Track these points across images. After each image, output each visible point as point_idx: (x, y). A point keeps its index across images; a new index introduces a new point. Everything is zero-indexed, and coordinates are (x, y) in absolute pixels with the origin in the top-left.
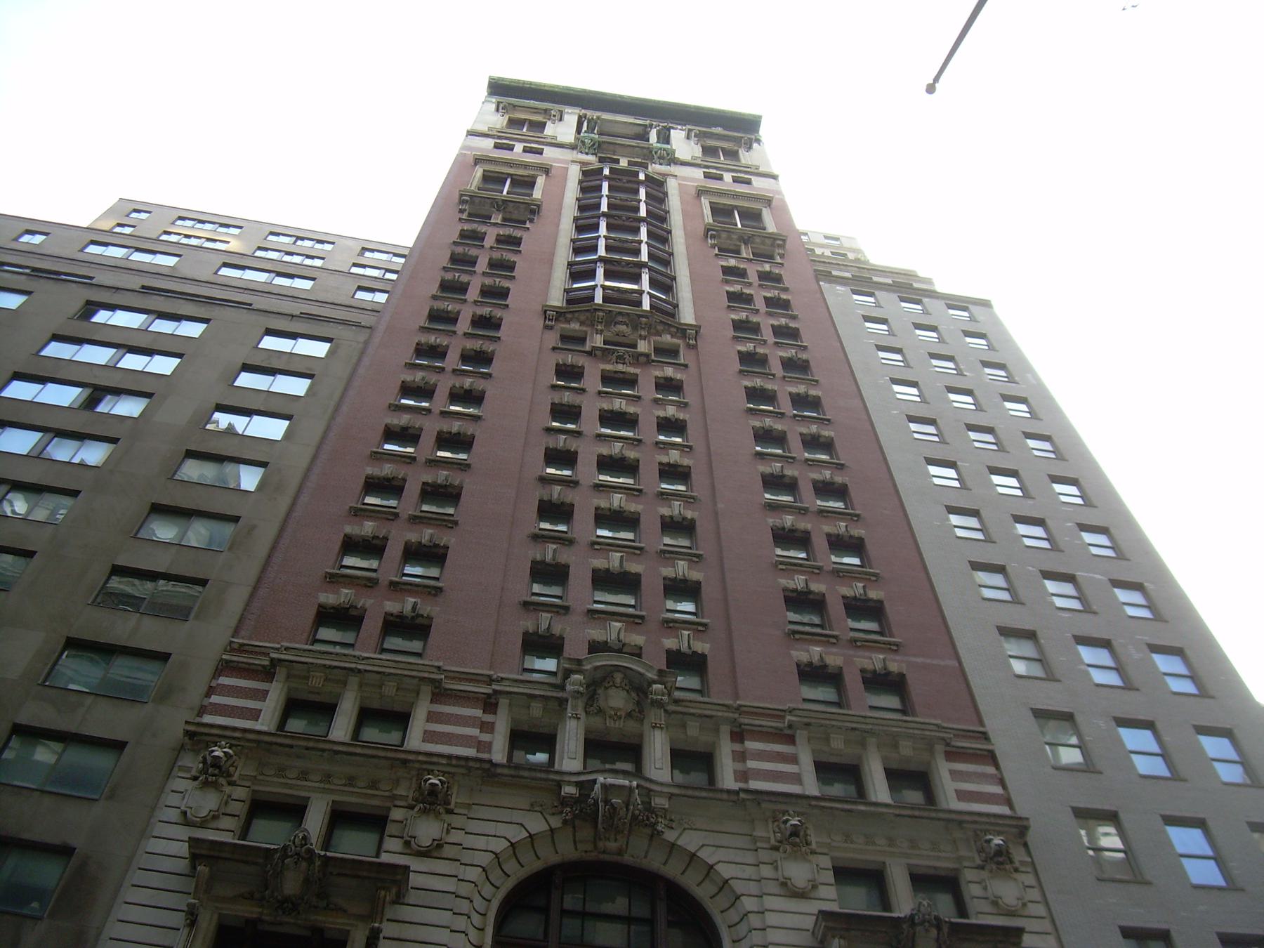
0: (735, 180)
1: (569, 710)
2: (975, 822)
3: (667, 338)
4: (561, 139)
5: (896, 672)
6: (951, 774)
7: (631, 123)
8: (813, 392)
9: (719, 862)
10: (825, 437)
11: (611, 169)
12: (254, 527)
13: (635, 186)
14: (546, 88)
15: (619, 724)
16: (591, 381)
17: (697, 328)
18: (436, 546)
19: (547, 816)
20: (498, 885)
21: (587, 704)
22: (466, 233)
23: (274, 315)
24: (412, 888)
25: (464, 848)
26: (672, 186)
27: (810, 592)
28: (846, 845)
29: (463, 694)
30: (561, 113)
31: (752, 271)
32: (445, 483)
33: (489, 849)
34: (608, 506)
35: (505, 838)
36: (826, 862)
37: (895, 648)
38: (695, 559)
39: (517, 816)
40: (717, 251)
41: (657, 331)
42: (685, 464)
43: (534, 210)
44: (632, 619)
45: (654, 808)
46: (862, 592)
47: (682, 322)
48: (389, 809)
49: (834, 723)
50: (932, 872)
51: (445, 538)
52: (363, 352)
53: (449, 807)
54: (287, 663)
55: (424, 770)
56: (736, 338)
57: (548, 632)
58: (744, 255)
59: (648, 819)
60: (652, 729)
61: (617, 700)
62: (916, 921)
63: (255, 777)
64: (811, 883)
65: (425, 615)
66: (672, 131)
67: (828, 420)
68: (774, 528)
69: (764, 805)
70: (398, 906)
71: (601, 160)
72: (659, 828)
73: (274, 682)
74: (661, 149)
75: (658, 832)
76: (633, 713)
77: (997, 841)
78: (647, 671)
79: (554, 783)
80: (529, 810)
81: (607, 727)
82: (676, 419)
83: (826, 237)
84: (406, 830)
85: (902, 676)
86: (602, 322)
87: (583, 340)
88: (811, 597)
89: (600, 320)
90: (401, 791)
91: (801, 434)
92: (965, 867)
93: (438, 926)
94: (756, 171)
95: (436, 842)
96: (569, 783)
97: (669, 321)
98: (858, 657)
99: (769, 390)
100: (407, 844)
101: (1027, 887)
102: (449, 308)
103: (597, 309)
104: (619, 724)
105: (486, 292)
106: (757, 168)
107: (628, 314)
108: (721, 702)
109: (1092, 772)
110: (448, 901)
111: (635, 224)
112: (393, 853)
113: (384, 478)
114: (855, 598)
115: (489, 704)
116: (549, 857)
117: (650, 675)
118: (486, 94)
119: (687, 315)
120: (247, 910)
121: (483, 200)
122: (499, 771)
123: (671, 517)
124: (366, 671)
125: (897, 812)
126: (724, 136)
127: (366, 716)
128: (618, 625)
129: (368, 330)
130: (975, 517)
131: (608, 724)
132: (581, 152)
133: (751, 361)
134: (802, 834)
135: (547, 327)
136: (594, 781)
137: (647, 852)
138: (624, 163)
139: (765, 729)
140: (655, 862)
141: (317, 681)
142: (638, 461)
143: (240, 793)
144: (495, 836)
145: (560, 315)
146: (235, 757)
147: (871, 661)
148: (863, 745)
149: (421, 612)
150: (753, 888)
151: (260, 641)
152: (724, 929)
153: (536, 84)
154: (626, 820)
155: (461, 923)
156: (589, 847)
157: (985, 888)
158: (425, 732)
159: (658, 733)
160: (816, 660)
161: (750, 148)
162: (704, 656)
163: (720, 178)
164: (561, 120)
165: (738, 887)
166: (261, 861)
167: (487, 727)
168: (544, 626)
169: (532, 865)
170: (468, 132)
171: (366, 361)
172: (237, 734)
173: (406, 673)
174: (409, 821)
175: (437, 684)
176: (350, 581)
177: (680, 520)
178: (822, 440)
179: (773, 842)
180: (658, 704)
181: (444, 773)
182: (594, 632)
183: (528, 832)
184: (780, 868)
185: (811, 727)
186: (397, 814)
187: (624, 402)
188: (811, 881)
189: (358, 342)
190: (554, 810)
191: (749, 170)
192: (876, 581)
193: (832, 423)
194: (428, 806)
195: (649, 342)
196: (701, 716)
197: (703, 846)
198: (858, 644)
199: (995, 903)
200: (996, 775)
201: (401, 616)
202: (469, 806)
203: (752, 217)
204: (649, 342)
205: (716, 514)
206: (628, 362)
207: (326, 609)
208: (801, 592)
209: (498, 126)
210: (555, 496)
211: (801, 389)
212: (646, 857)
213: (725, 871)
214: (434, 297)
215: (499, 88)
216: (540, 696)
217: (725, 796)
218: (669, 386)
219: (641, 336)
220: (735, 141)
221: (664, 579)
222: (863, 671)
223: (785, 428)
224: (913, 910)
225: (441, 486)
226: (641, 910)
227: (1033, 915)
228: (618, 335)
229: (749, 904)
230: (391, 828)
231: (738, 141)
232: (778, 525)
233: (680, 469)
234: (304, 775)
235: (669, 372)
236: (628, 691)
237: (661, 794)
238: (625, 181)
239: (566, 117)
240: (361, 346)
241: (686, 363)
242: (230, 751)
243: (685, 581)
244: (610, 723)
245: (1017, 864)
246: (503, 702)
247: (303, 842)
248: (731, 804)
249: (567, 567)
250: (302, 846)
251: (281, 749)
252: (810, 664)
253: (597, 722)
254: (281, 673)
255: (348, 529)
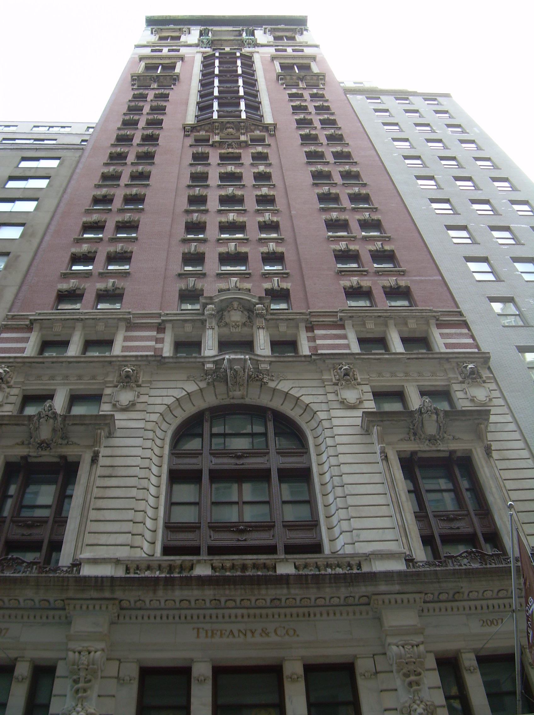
0: (294, 51)
1: (207, 325)
2: (456, 358)
3: (257, 133)
4: (189, 42)
5: (404, 286)
6: (440, 335)
7: (231, 31)
8: (346, 150)
9: (302, 395)
10: (354, 171)
11: (220, 53)
12: (18, 256)
13: (234, 60)
14: (179, 18)
15: (238, 330)
16: (214, 159)
17: (275, 125)
18: (126, 252)
19: (197, 382)
20: (171, 423)
21: (218, 321)
22: (136, 96)
23: (26, 150)
24: (118, 428)
25: (148, 405)
26: (257, 59)
27: (350, 250)
28: (379, 378)
29: (145, 325)
30: (189, 29)
31: (306, 94)
32: (129, 220)
33: (164, 403)
34: (226, 220)
35: (173, 396)
36: (367, 388)
37: (402, 273)
38: (279, 241)
39: (180, 385)
40: (284, 86)
41: (251, 129)
42: (271, 194)
43: (175, 79)
44: (244, 276)
45: (261, 370)
46: (381, 246)
47: (266, 123)
48: (103, 389)
49: (367, 314)
50: (433, 389)
51: (129, 247)
52: (78, 162)
53: (138, 383)
54: (40, 321)
55: (122, 365)
56: (297, 128)
57: (194, 288)
58: (301, 86)
59: (258, 377)
60: (258, 330)
61: (236, 317)
62: (423, 412)
63: (23, 382)
64: (358, 400)
65: (120, 287)
66: (255, 31)
67: (356, 163)
68: (326, 220)
69: (327, 361)
70: (110, 439)
71: (214, 50)
72: (265, 381)
73: (33, 332)
74: (248, 39)
75: (264, 383)
76: (246, 323)
77: (470, 366)
78: (252, 298)
79: (201, 364)
80: (187, 380)
81: (231, 332)
82: (265, 172)
83: (355, 83)
84: (113, 398)
85: (408, 288)
86: (218, 129)
87: (208, 140)
88: (351, 253)
89: (217, 128)
90: (109, 379)
91: (340, 172)
92: (453, 383)
93: (134, 447)
94: (306, 44)
95: (131, 403)
96: (209, 362)
97: (258, 123)
98: (381, 280)
99: (319, 152)
100: (114, 405)
101: (491, 390)
102: (128, 133)
103: (215, 121)
104: (238, 330)
105: (149, 123)
106: (306, 43)
107: (233, 122)
108: (298, 312)
109: (528, 327)
110: (141, 433)
111: (235, 78)
112: (106, 408)
113: (93, 222)
114: (377, 251)
115: (160, 328)
116: (200, 404)
117: (254, 300)
118: (145, 26)
119: (268, 119)
120: (22, 451)
121: (145, 77)
122: (167, 360)
123: (265, 222)
124: (86, 319)
125: (408, 356)
126: (286, 29)
127: (88, 344)
128: (236, 279)
129: (81, 150)
130: (465, 230)
131: (232, 331)
132: (202, 47)
133: (307, 139)
134: (351, 374)
135: (186, 136)
136: (224, 359)
137: (260, 395)
138: (227, 49)
139: (326, 323)
140: (265, 400)
141: (58, 328)
142: (244, 196)
143: (15, 391)
144: (167, 396)
145: (193, 128)
146: (10, 373)
147: (388, 282)
148: (386, 325)
149: (118, 286)
150: (324, 407)
151: (23, 312)
152: (308, 432)
153: (173, 16)
154: (244, 378)
155: (149, 444)
156: (225, 396)
157: (466, 393)
158: (123, 347)
159: (261, 331)
160: (355, 284)
161: (302, 34)
162: (288, 290)
163: (285, 51)
164: (189, 33)
165: (315, 407)
166: (26, 423)
167: (161, 341)
168: (191, 285)
169: (190, 410)
170: (135, 46)
171: (80, 166)
172: (11, 360)
173: (110, 317)
174: (115, 393)
175: (128, 321)
176: (77, 274)
177: (270, 223)
178: (352, 173)
179: (334, 380)
180: (261, 316)
181: (134, 366)
182: (221, 285)
183: (186, 391)
184: (339, 394)
185: (354, 318)
186: (108, 391)
187: (233, 167)
188: (358, 399)
189: (76, 157)
190: (201, 378)
191: (301, 44)
192: (389, 240)
193: (358, 164)
194: (125, 384)
195: (247, 136)
196: (287, 320)
197: (292, 388)
198: (380, 273)
199: (472, 400)
200: (468, 333)
201: (106, 290)
202: (150, 382)
203: (307, 67)
204: (247, 136)
205: (291, 217)
206: (235, 147)
207: (62, 292)
208: (344, 251)
209: (153, 40)
210: (195, 219)
211: (339, 149)
212: (259, 398)
213: (306, 400)
214: (119, 129)
215: (152, 22)
216: (190, 320)
217: (303, 359)
218: (260, 157)
219: (241, 133)
220: (292, 31)
221: (262, 253)
222: (384, 287)
223: (330, 169)
224: (420, 405)
225: (126, 222)
226: (259, 429)
227: (496, 405)
228: (228, 134)
229: (322, 415)
230: (104, 399)
231: (294, 31)
232: (328, 218)
233: (269, 198)
234: (52, 378)
235: (260, 149)
236: (242, 311)
237: (264, 362)
238: (228, 58)
239: (192, 32)
240: (77, 158)
241: (269, 143)
242: (7, 369)
243: (274, 253)
244: (233, 330)
245: (484, 379)
246: (169, 326)
247: (50, 409)
248: (307, 363)
249: (203, 254)
250: (49, 411)
251: (38, 365)
252: (352, 287)
253: (225, 330)
254: (36, 326)
255: (73, 250)
